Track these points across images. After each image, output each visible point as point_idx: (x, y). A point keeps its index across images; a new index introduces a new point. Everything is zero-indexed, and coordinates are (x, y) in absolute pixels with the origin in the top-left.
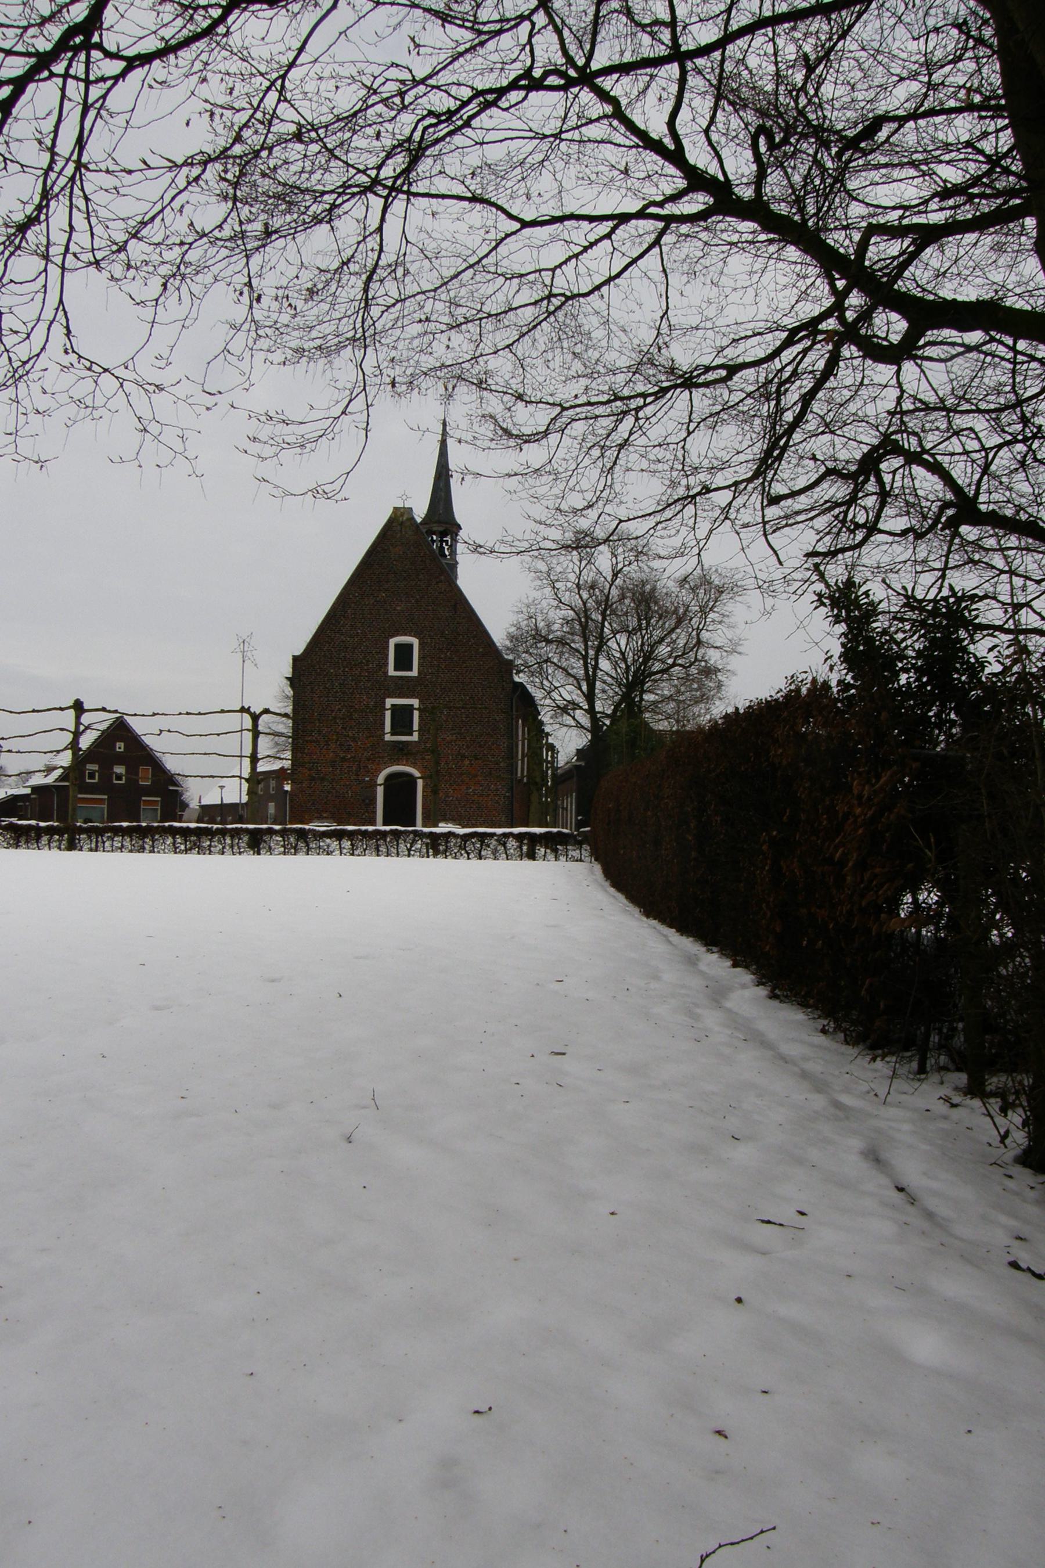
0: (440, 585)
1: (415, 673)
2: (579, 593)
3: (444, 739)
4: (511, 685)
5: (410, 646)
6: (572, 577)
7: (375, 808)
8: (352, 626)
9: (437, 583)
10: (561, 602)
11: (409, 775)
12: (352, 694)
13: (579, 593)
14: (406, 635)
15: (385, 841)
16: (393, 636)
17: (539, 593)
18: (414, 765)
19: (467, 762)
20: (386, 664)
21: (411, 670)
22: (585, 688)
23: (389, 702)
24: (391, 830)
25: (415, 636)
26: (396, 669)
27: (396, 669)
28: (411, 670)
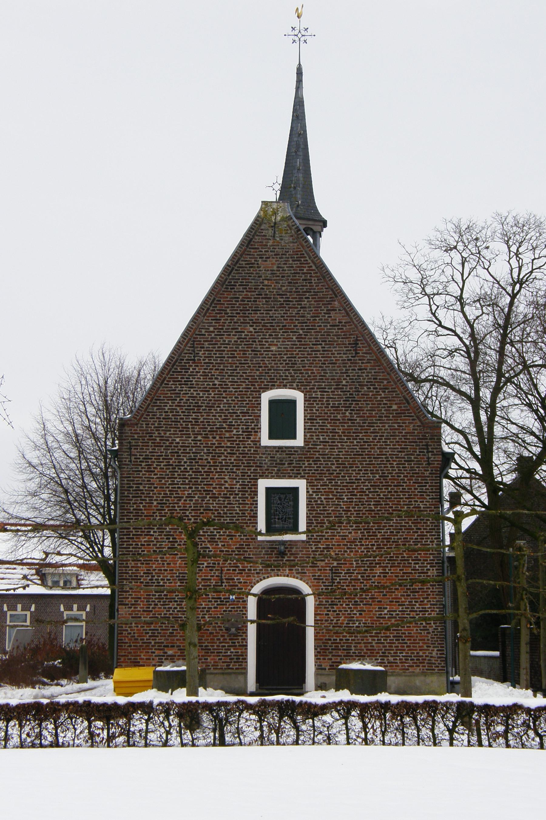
0: (333, 314)
1: (299, 441)
2: (462, 311)
3: (344, 537)
4: (440, 458)
5: (292, 403)
6: (454, 289)
7: (245, 640)
8: (205, 375)
9: (329, 312)
10: (440, 325)
11: (296, 591)
12: (208, 473)
13: (462, 311)
14: (285, 387)
15: (415, 719)
16: (266, 389)
17: (406, 312)
18: (301, 576)
19: (378, 571)
20: (257, 430)
21: (294, 437)
22: (477, 449)
23: (263, 484)
24: (426, 703)
25: (299, 389)
26: (271, 437)
27: (271, 437)
28: (294, 437)
